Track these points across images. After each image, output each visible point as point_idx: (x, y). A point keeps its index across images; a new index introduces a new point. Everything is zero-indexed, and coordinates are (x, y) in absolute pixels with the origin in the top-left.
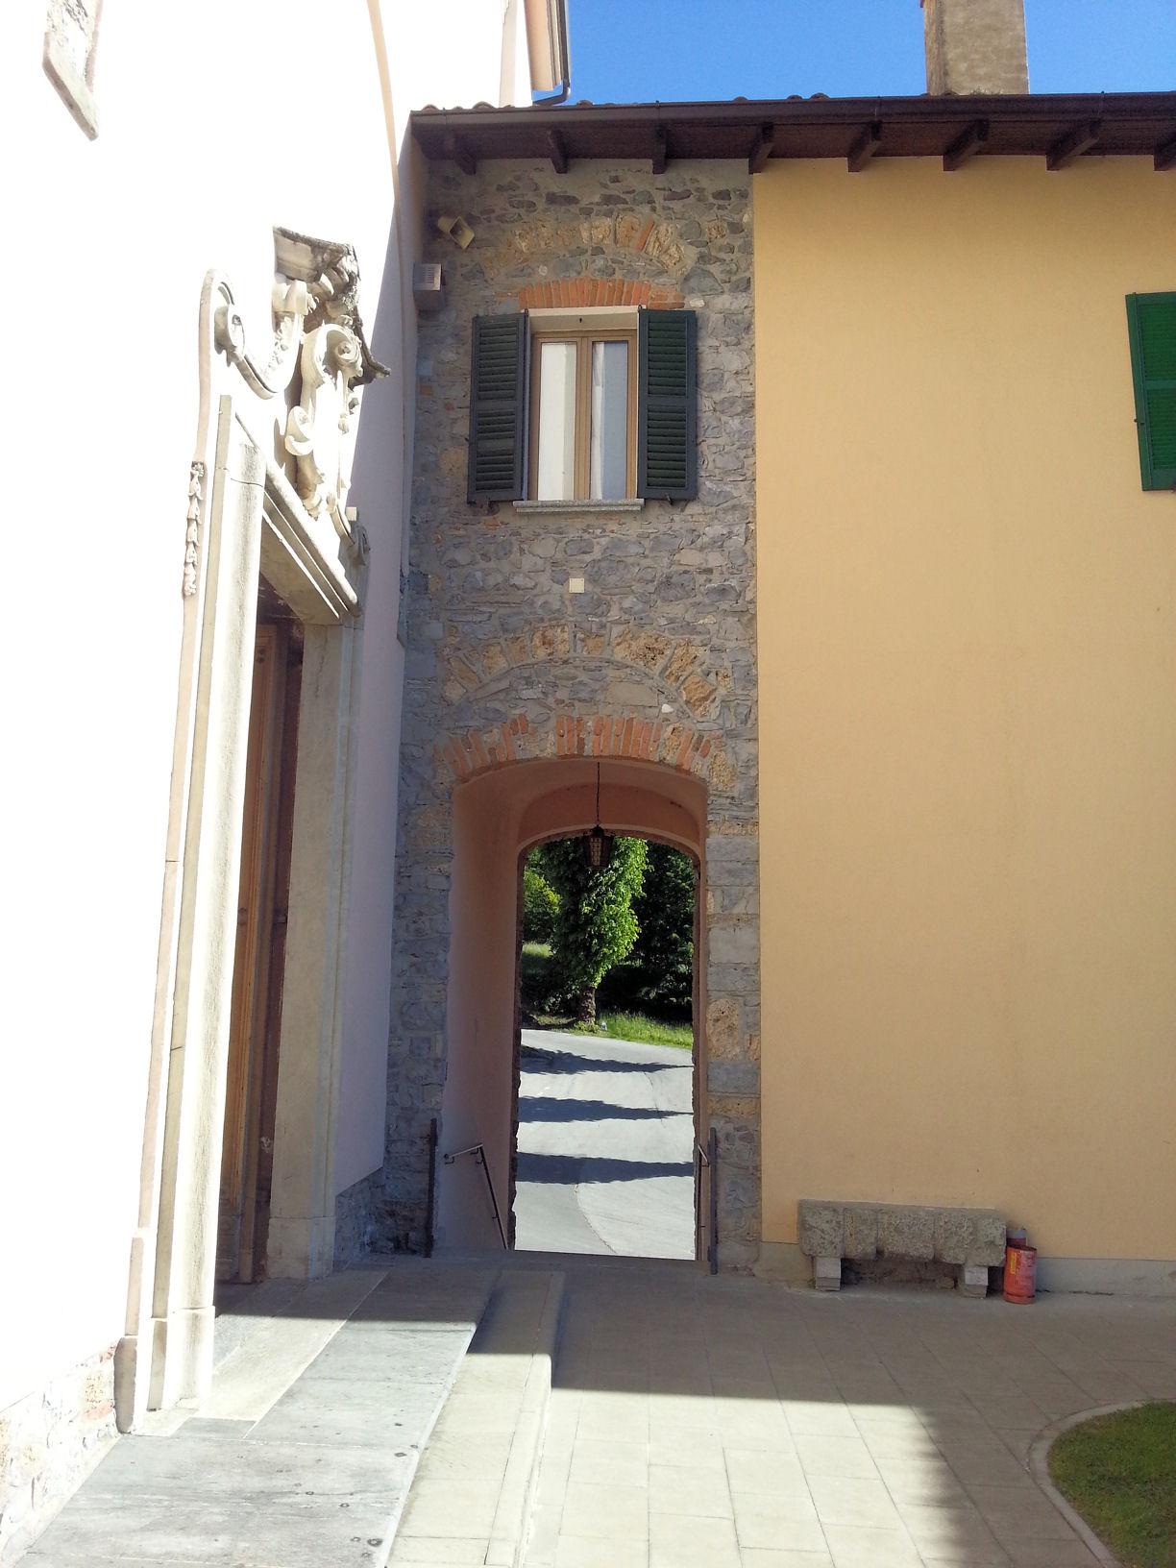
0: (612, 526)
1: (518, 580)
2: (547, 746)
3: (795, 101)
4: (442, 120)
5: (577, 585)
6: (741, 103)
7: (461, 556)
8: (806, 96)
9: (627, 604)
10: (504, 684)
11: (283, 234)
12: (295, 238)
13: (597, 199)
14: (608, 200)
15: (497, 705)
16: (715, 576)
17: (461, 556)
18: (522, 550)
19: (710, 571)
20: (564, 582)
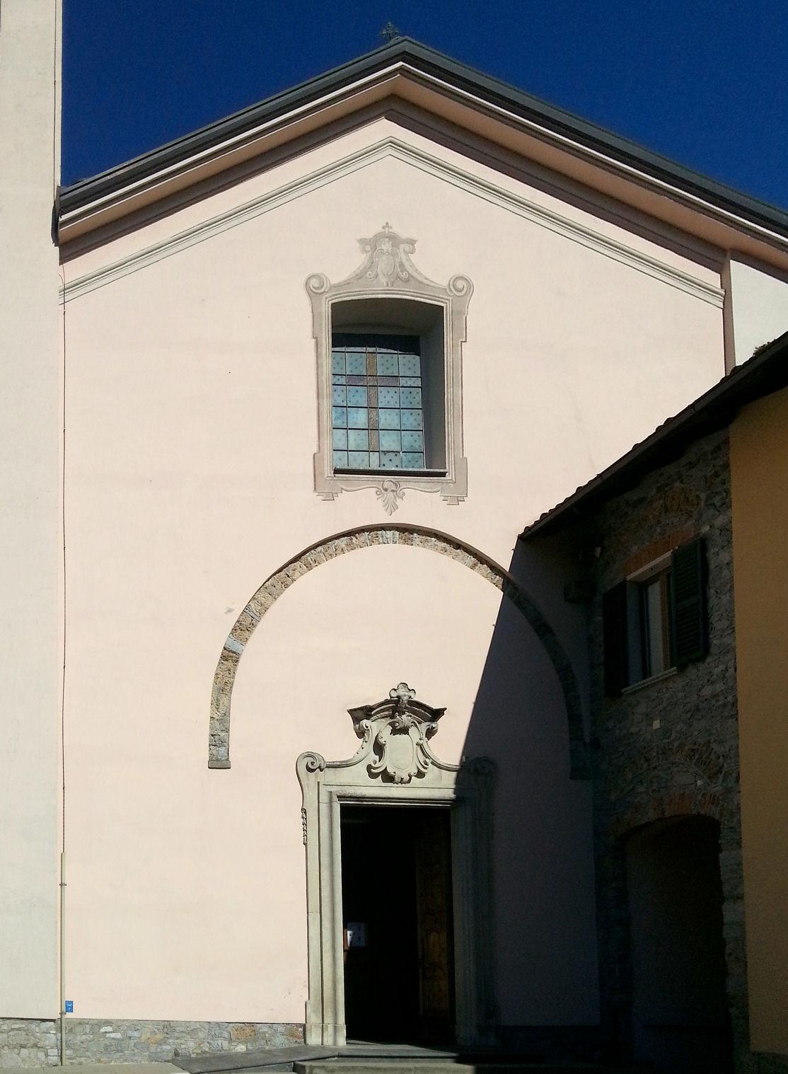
0: (671, 685)
1: (633, 730)
2: (651, 815)
3: (659, 429)
4: (587, 490)
5: (656, 724)
6: (636, 446)
7: (610, 725)
8: (547, 511)
9: (679, 727)
10: (631, 787)
11: (351, 712)
12: (355, 710)
13: (654, 492)
14: (659, 489)
15: (628, 799)
16: (721, 698)
17: (610, 725)
18: (633, 713)
19: (716, 695)
20: (651, 725)
